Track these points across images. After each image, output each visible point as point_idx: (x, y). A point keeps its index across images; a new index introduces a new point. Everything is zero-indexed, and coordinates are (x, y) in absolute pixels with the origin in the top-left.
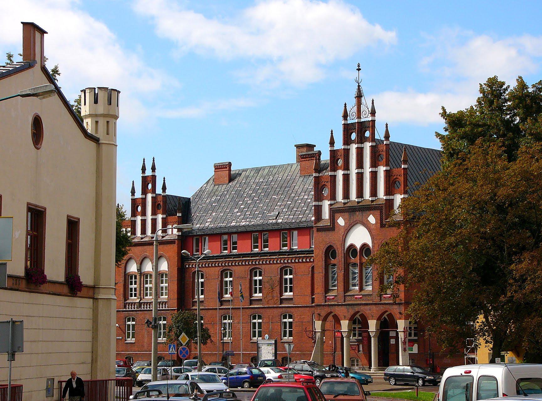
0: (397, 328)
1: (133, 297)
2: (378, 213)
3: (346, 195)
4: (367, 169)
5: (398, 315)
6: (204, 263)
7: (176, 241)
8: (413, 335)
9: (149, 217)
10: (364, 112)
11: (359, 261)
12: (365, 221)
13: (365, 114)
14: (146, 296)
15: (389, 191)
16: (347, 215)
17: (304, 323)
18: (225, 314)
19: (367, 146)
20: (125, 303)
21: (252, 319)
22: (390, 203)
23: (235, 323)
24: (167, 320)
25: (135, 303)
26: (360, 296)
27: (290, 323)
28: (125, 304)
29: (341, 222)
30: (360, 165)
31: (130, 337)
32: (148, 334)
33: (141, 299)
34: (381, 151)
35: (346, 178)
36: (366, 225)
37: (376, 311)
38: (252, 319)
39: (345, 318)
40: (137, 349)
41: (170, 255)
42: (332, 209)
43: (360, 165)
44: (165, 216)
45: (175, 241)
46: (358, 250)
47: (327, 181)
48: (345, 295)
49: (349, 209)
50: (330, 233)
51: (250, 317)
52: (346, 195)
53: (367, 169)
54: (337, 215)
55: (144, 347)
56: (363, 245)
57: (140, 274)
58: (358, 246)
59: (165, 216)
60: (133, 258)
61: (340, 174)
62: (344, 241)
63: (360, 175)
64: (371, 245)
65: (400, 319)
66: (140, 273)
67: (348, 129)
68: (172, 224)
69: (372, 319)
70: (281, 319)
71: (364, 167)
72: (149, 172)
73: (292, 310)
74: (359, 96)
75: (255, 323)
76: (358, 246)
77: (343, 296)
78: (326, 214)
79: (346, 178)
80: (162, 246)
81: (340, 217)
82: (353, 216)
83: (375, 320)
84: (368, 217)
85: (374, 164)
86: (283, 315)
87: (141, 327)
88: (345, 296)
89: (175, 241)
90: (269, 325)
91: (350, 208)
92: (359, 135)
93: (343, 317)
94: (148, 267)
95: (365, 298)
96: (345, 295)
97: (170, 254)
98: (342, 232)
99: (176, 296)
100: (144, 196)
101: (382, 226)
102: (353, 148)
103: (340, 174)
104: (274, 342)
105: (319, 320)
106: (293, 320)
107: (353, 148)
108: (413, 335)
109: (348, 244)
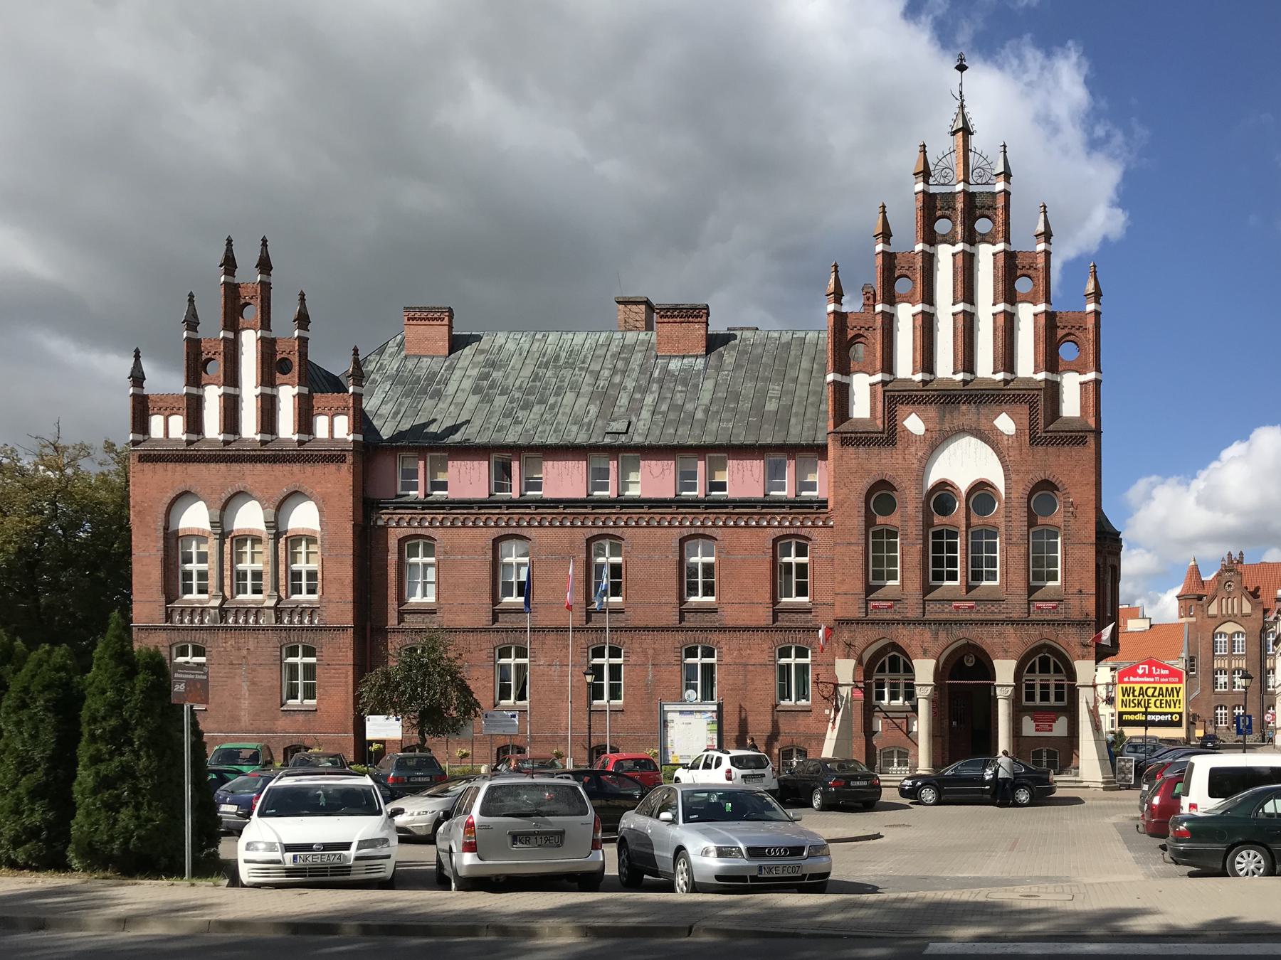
0: (995, 680)
1: (194, 596)
2: (1024, 410)
3: (927, 360)
4: (987, 307)
5: (1078, 650)
6: (473, 518)
7: (350, 458)
8: (1052, 698)
9: (250, 389)
10: (978, 170)
11: (963, 521)
12: (984, 425)
13: (980, 176)
14: (691, 595)
15: (1051, 361)
16: (932, 411)
17: (751, 668)
18: (181, 642)
19: (986, 255)
20: (167, 608)
21: (284, 655)
22: (1053, 391)
23: (539, 665)
24: (317, 654)
25: (203, 609)
26: (968, 604)
27: (309, 669)
28: (169, 609)
29: (914, 424)
30: (967, 291)
31: (300, 695)
32: (250, 688)
33: (224, 599)
34: (1028, 267)
35: (927, 325)
36: (990, 437)
37: (1018, 640)
38: (284, 655)
39: (925, 654)
40: (216, 726)
41: (329, 490)
42: (887, 394)
43: (967, 291)
44: (305, 390)
45: (344, 455)
46: (964, 495)
47: (867, 327)
48: (1031, 599)
49: (938, 396)
50: (885, 452)
51: (492, 651)
52: (927, 360)
53: (987, 307)
54: (901, 409)
55: (239, 721)
56: (943, 482)
57: (220, 534)
58: (963, 484)
59: (305, 390)
60: (251, 497)
61: (906, 314)
62: (923, 471)
63: (968, 319)
64: (1000, 484)
65: (1083, 657)
66: (219, 531)
67: (932, 207)
68: (331, 413)
69: (1005, 658)
70: (775, 657)
71: (975, 302)
72: (248, 275)
73: (714, 637)
74: (966, 131)
75: (293, 667)
76: (963, 485)
77: (922, 601)
78: (861, 407)
79: (927, 325)
80: (148, 467)
81: (911, 413)
82: (951, 413)
83: (1012, 659)
84: (996, 418)
85: (1009, 295)
86: (177, 649)
87: (227, 670)
88: (867, 602)
89: (344, 455)
90: (647, 671)
91: (944, 392)
92: (966, 221)
93: (920, 650)
94: (250, 517)
95: (981, 608)
96: (1031, 599)
97: (327, 488)
98: (915, 451)
99: (349, 595)
100: (231, 335)
101: (1034, 440)
102: (945, 255)
103: (906, 314)
104: (715, 708)
105: (848, 657)
106: (317, 660)
107: (945, 255)
108: (1052, 698)
109: (933, 479)
